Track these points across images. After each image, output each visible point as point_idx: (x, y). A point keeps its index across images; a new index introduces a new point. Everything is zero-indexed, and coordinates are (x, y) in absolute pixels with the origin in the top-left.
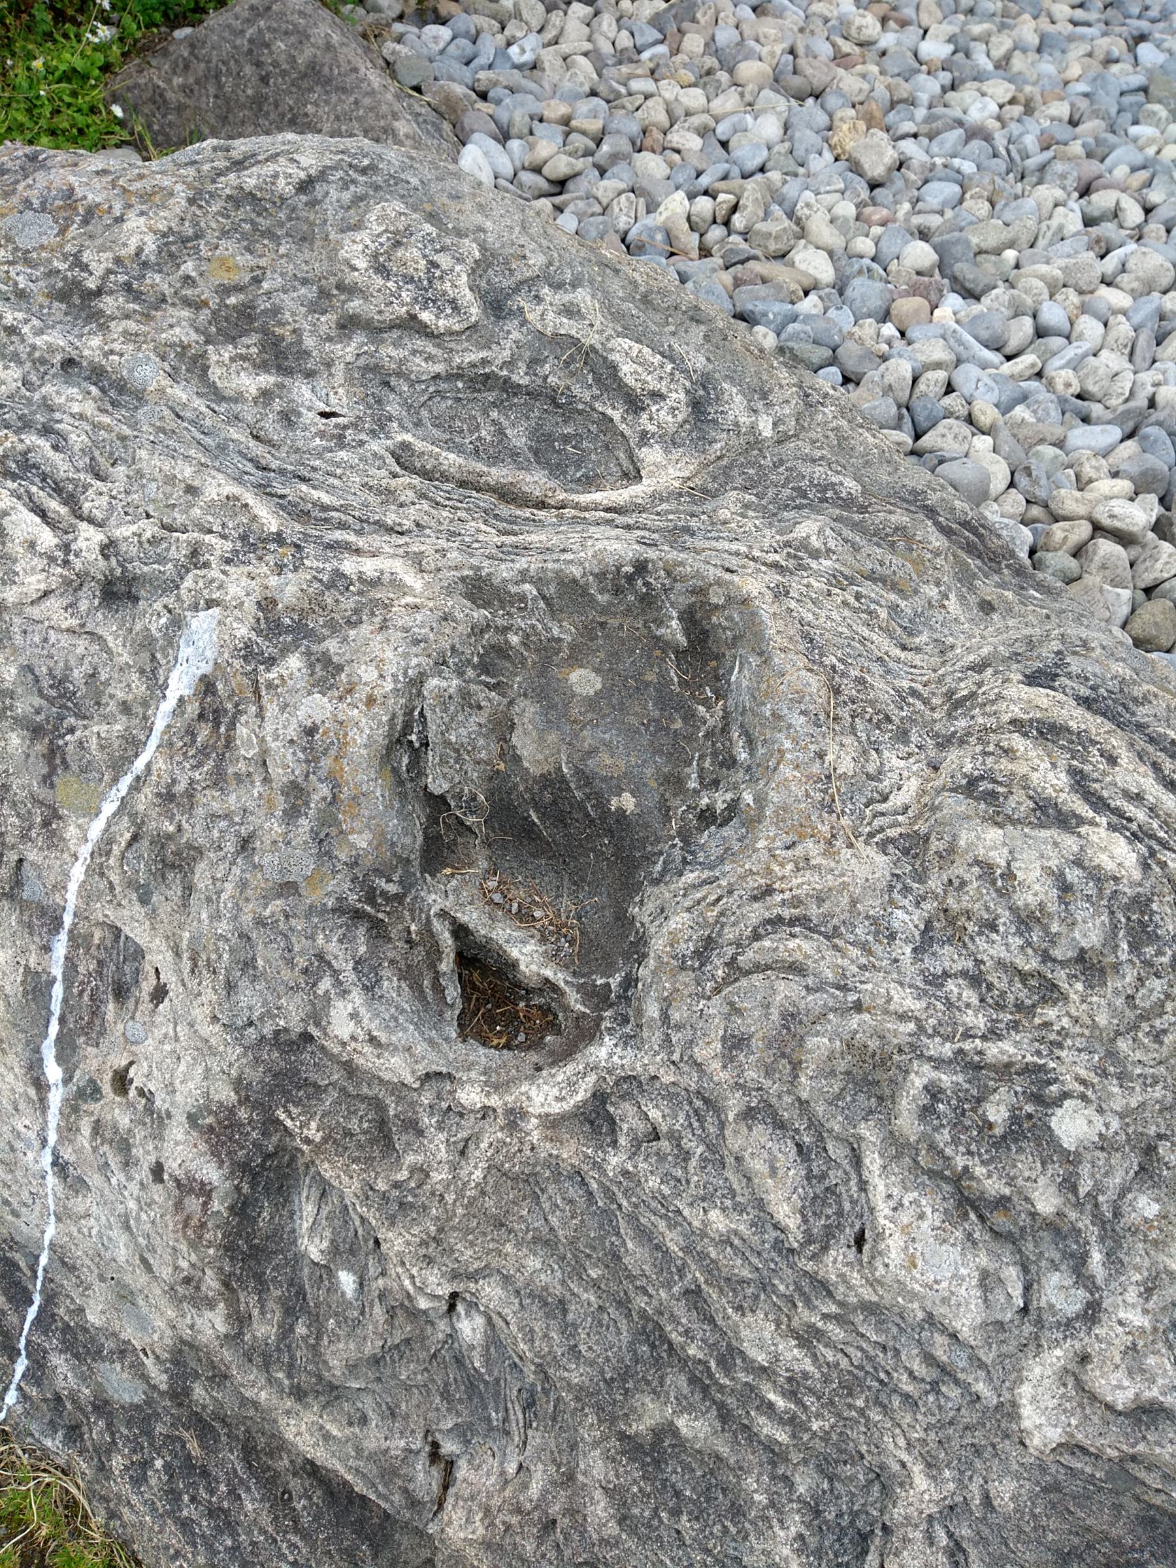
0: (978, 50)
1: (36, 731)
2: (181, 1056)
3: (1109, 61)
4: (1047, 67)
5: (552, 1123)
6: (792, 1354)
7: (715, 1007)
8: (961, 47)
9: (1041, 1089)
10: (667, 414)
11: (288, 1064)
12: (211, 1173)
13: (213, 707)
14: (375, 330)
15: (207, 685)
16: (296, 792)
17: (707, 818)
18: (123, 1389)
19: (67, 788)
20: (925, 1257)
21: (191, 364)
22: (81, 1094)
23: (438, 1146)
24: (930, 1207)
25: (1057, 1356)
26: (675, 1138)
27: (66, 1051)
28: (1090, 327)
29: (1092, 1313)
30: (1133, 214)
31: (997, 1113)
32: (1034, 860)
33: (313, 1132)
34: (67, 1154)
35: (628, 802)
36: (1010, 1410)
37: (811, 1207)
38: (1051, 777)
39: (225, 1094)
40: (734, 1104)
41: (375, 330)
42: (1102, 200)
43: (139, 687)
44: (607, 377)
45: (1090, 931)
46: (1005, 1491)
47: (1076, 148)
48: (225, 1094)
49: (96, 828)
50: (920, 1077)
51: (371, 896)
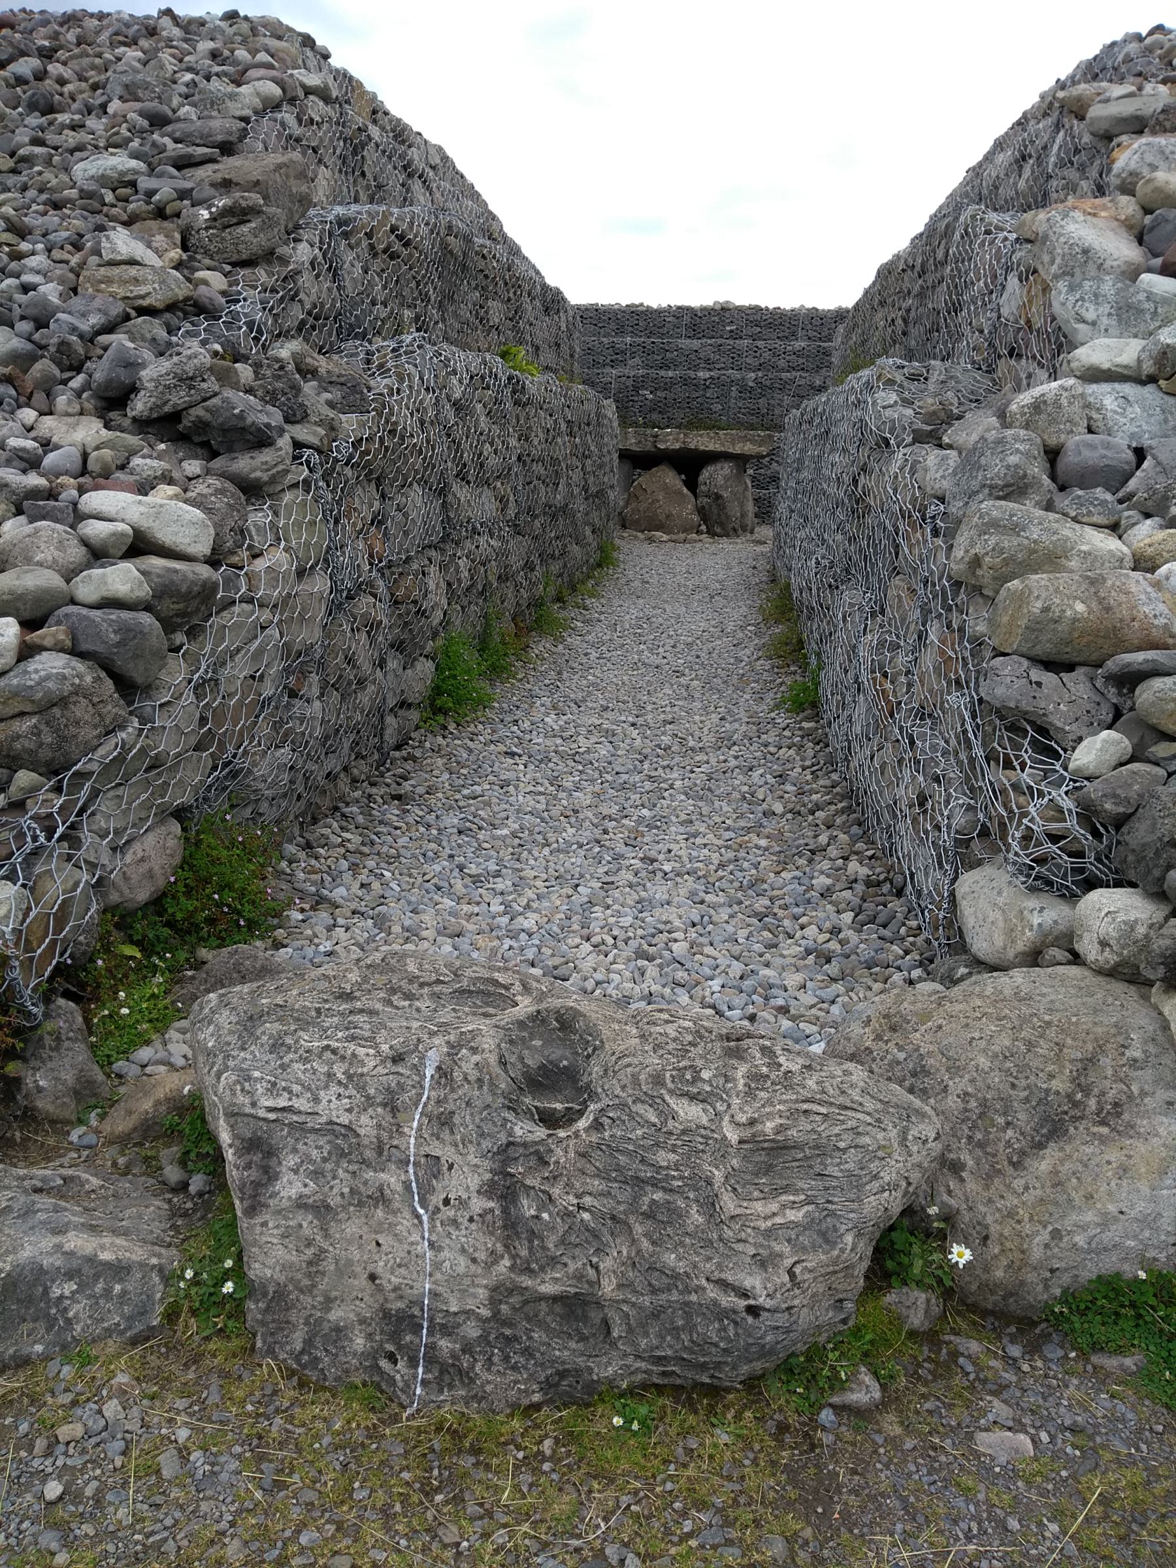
0: (514, 905)
1: (385, 1105)
2: (466, 1179)
3: (569, 897)
4: (545, 904)
5: (587, 1130)
6: (672, 1157)
7: (615, 1081)
8: (507, 906)
9: (697, 1072)
10: (518, 987)
11: (506, 1153)
12: (491, 1204)
13: (443, 1073)
14: (429, 984)
15: (439, 1068)
16: (480, 1081)
17: (588, 1056)
18: (472, 1331)
19: (401, 1117)
20: (690, 1112)
21: (389, 1003)
22: (434, 1213)
23: (559, 1152)
24: (685, 1101)
25: (727, 1118)
26: (619, 1118)
27: (423, 1203)
28: (616, 977)
29: (729, 1106)
30: (610, 941)
31: (688, 1077)
32: (671, 1030)
33: (521, 1170)
34: (434, 1238)
35: (565, 1063)
36: (725, 1138)
37: (659, 1116)
38: (666, 1016)
39: (488, 1176)
40: (630, 1100)
41: (429, 984)
42: (596, 939)
43: (417, 1078)
44: (496, 983)
45: (690, 1038)
46: (735, 1162)
47: (576, 927)
48: (488, 1176)
49: (415, 1124)
50: (668, 1075)
51: (510, 1101)
